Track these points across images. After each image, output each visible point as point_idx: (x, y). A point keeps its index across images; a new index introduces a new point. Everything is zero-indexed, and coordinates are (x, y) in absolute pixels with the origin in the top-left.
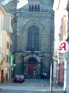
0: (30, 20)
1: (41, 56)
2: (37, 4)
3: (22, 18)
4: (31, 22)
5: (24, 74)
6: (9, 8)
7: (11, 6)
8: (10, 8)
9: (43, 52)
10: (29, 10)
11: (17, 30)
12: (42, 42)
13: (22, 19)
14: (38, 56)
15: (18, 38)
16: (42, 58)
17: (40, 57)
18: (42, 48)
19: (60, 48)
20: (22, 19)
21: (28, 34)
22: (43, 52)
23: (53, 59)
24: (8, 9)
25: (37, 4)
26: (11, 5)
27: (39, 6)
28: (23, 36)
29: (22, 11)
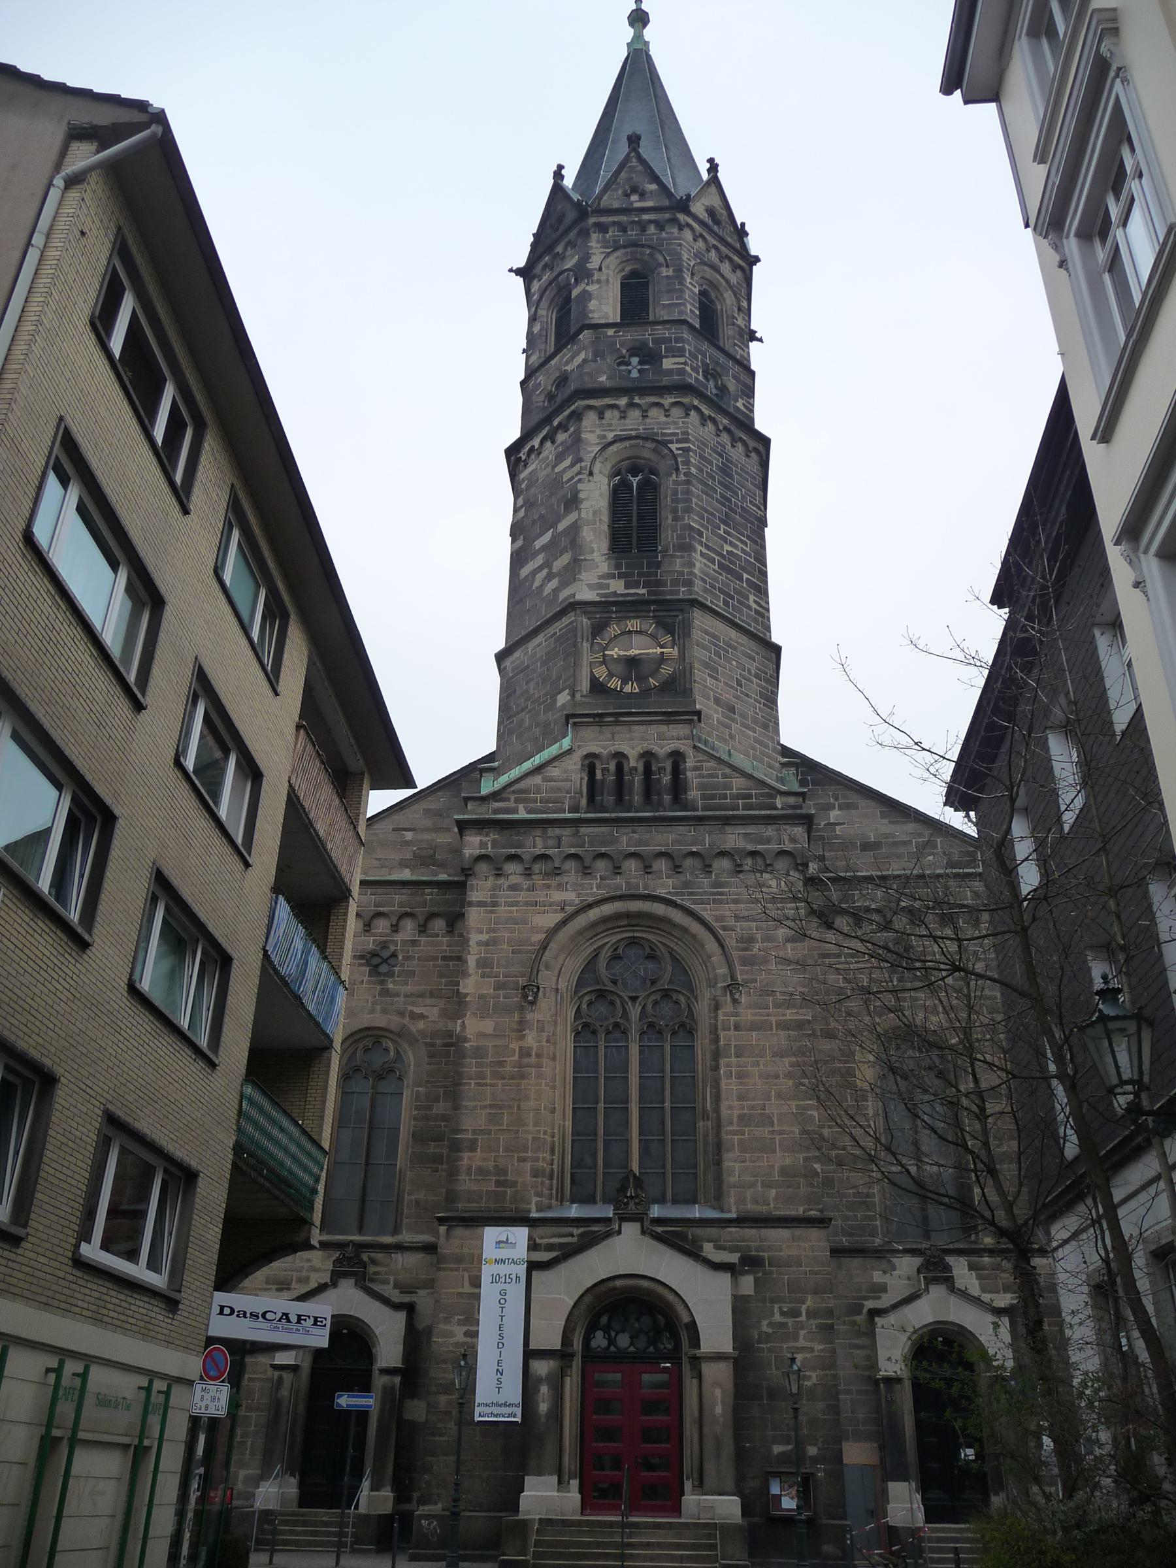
0: (594, 888)
1: (734, 1258)
2: (662, 749)
3: (513, 880)
4: (608, 909)
5: (656, 1211)
6: (409, 836)
7: (428, 823)
8: (427, 836)
9: (742, 1221)
10: (584, 802)
11: (470, 986)
12: (731, 1108)
13: (514, 888)
14: (952, 1289)
15: (470, 1066)
16: (747, 1284)
17: (725, 1278)
18: (734, 1165)
19: (294, 1319)
20: (514, 888)
21: (584, 1031)
22: (742, 1221)
23: (1073, 1359)
24: (408, 843)
25: (656, 749)
26: (427, 812)
27: (677, 771)
28: (525, 1053)
29: (515, 811)
